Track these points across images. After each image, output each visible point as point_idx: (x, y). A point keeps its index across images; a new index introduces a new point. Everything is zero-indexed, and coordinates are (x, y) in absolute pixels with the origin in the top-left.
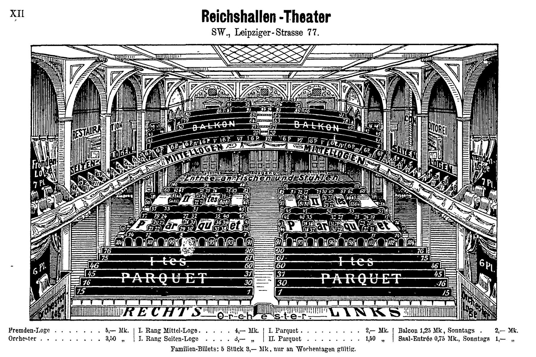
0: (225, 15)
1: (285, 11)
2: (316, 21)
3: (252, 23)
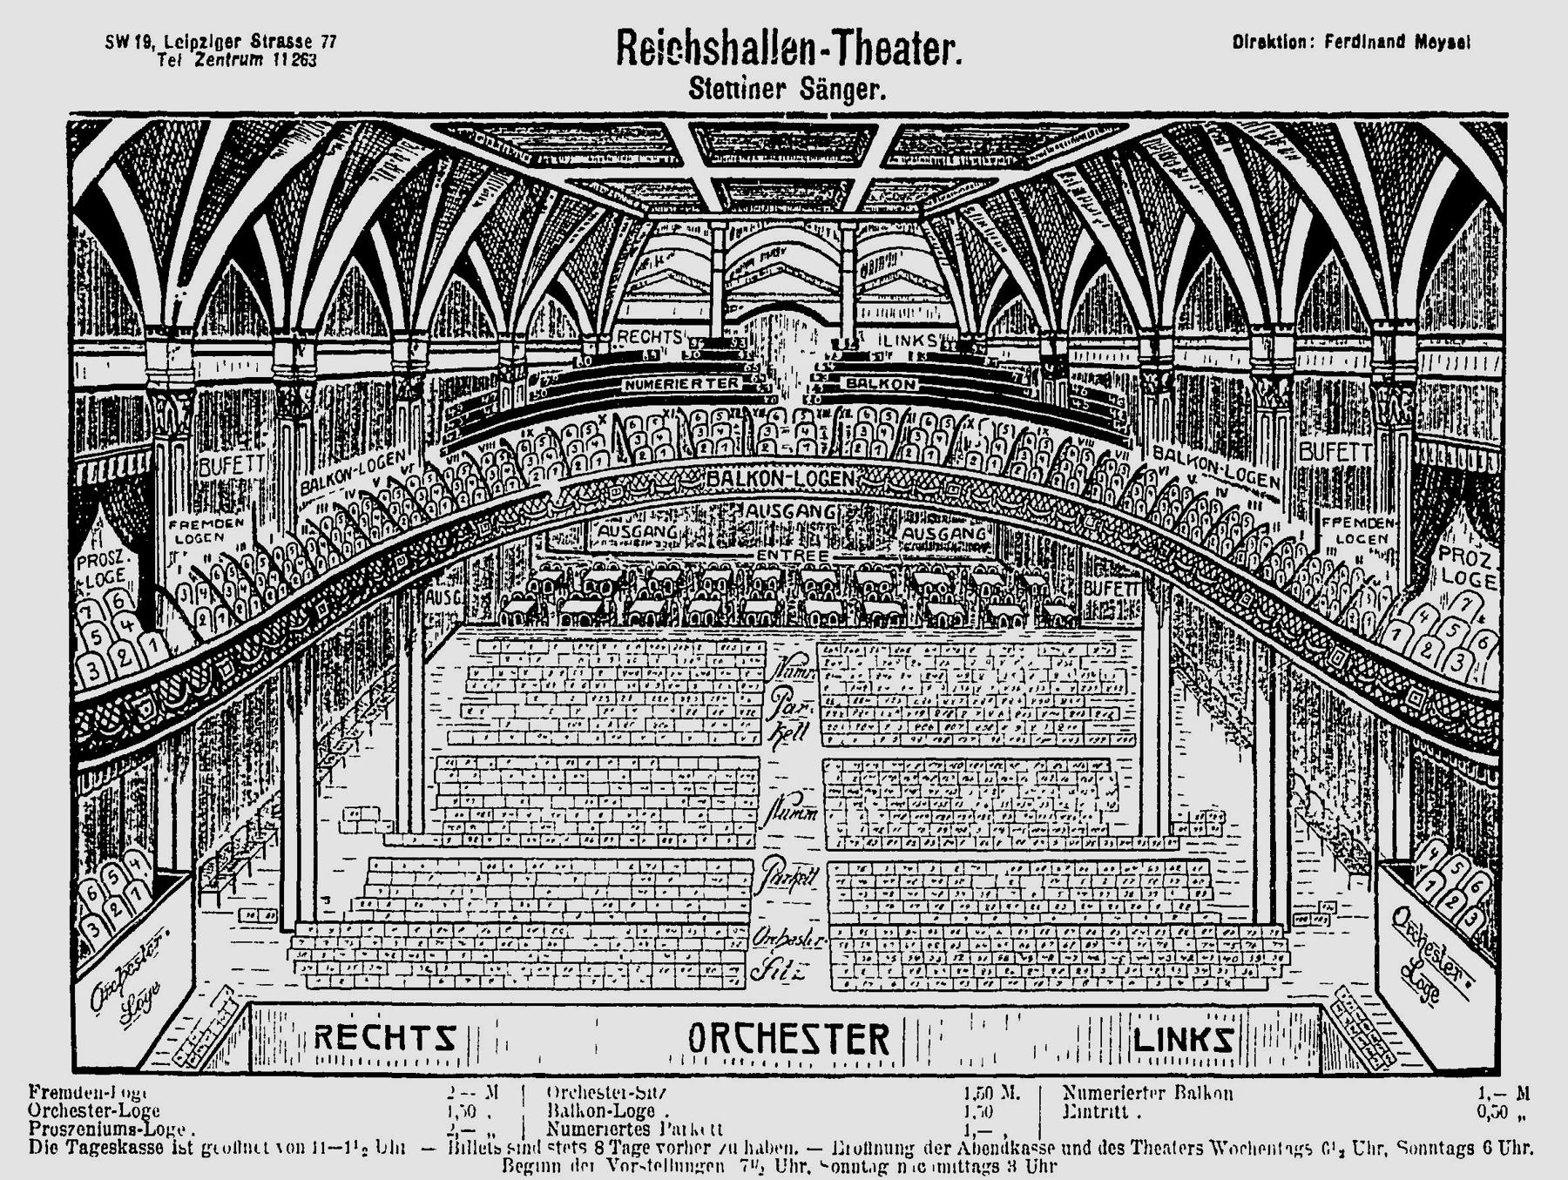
1: (835, 31)
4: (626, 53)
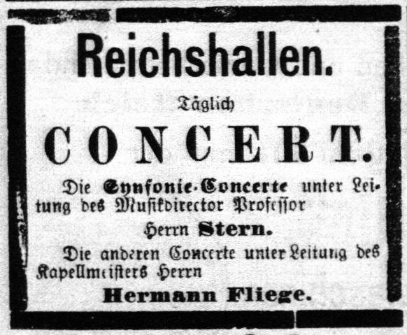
0: (155, 56)
2: (268, 257)
4: (89, 62)
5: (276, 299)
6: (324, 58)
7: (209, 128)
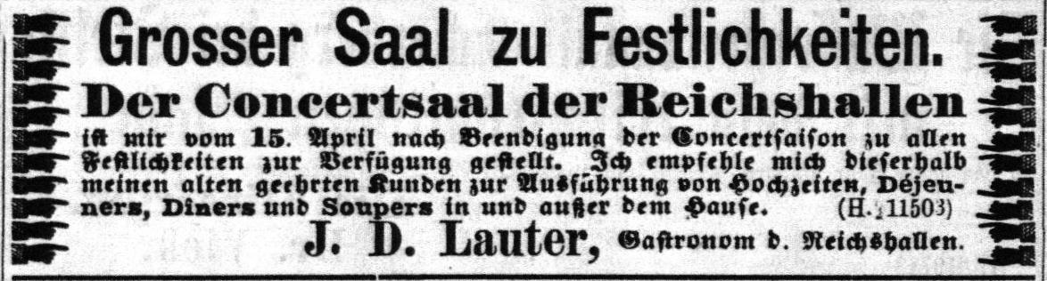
0: (742, 38)
3: (390, 67)
5: (322, 110)
6: (931, 42)
7: (228, 85)
